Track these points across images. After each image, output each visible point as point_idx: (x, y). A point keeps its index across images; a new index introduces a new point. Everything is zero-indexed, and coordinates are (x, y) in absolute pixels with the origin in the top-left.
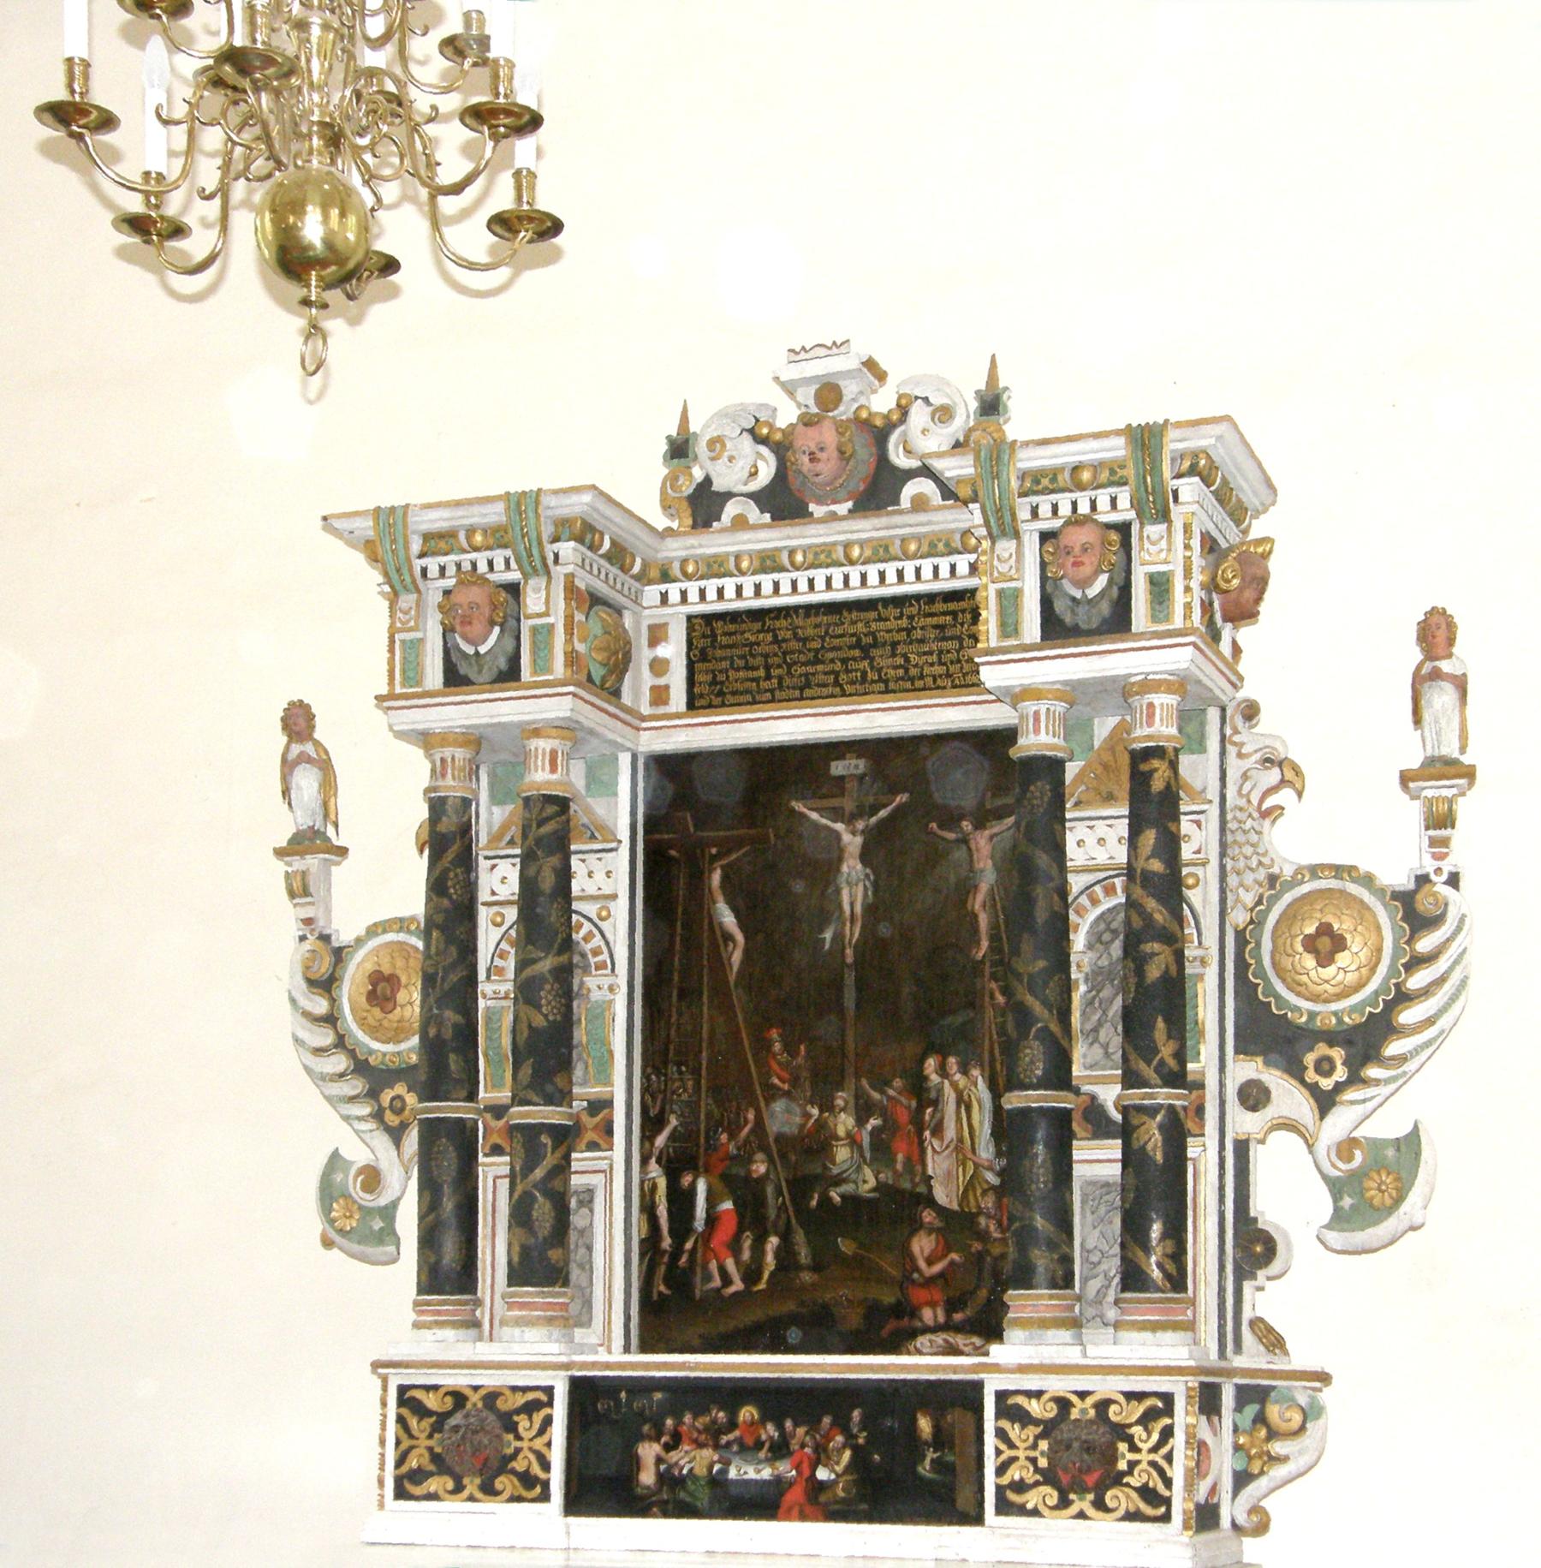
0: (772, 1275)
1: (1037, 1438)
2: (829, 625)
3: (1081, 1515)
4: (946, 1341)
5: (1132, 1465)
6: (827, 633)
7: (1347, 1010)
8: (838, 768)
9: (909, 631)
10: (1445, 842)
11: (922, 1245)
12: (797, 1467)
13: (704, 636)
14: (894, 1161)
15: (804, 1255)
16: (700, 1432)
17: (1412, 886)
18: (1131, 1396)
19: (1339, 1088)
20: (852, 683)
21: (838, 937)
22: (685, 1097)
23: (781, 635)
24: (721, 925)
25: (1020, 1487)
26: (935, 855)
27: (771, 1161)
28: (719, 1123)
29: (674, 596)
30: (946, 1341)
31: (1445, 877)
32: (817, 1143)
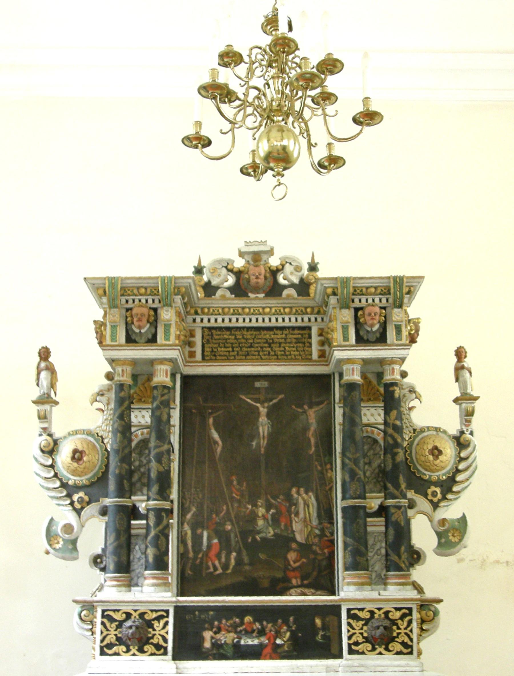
0: (234, 567)
1: (363, 625)
2: (256, 335)
3: (380, 653)
4: (301, 591)
5: (399, 634)
6: (255, 337)
7: (442, 475)
8: (257, 384)
9: (285, 339)
10: (470, 421)
11: (292, 556)
12: (269, 639)
13: (209, 335)
14: (281, 525)
15: (246, 559)
16: (229, 627)
17: (458, 435)
18: (397, 609)
19: (440, 501)
20: (265, 355)
21: (258, 444)
22: (199, 500)
23: (238, 337)
24: (213, 438)
25: (357, 644)
26: (295, 417)
27: (233, 524)
28: (212, 511)
29: (198, 320)
30: (301, 591)
31: (469, 432)
32: (253, 518)
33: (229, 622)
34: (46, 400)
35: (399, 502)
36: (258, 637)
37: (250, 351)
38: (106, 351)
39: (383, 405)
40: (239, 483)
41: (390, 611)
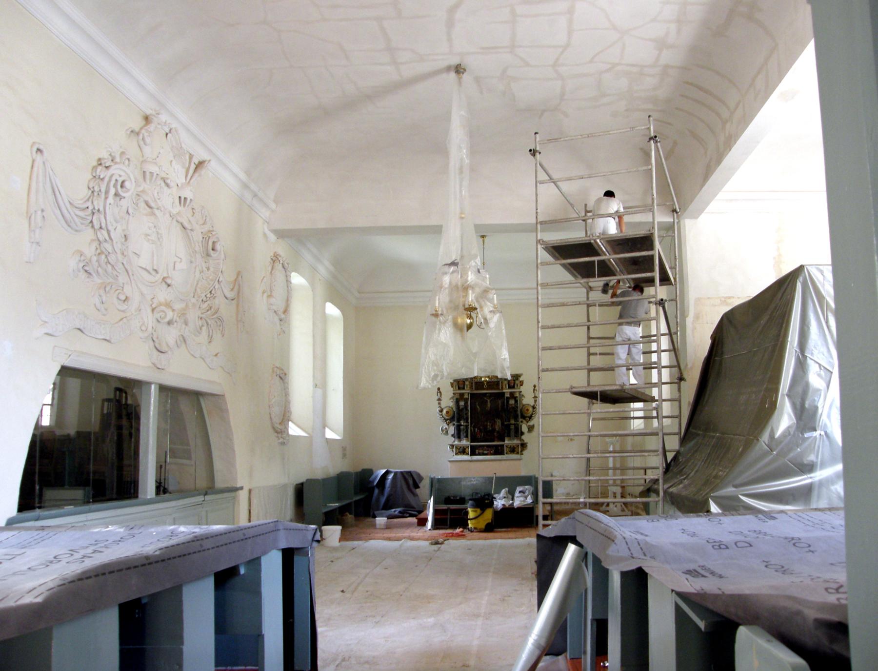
34: (439, 400)
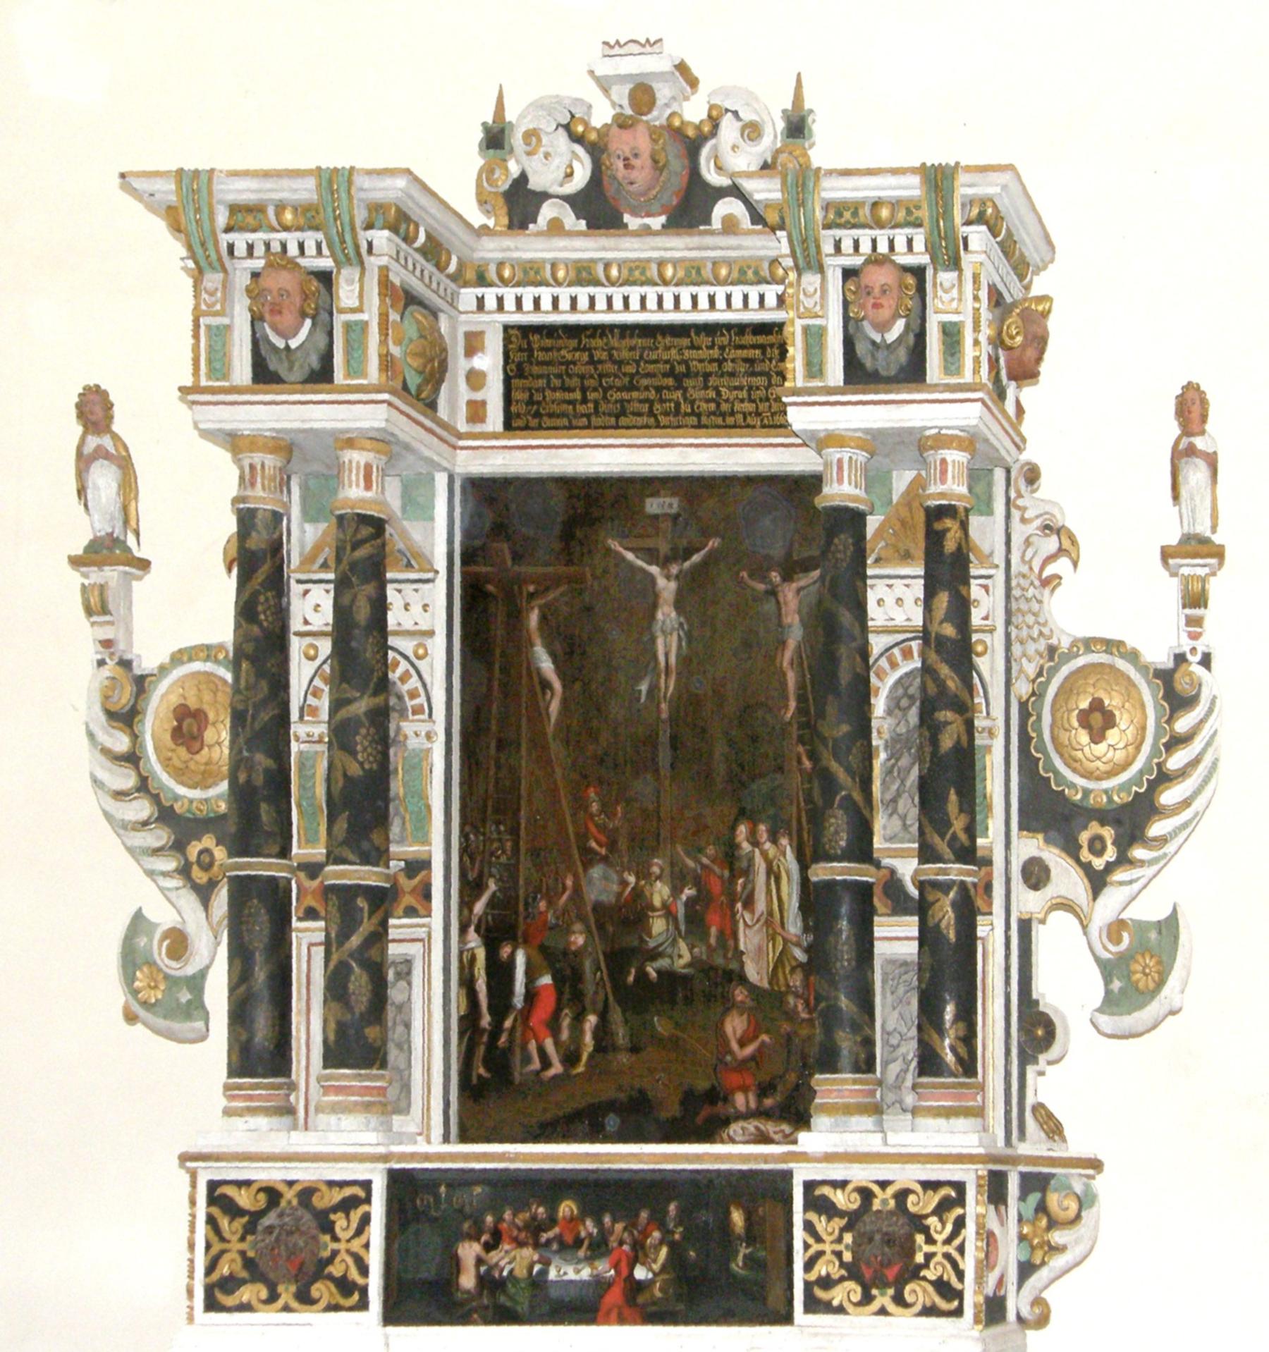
1: (843, 1230)
2: (643, 349)
3: (883, 1311)
4: (757, 1128)
5: (929, 1257)
6: (641, 357)
7: (1112, 789)
8: (653, 506)
9: (720, 362)
11: (735, 1025)
12: (616, 1266)
13: (521, 350)
17: (1171, 665)
19: (1109, 868)
20: (666, 414)
21: (653, 689)
23: (598, 355)
24: (538, 670)
25: (827, 1283)
27: (588, 931)
28: (538, 890)
30: (757, 1128)
31: (1198, 657)
32: (631, 913)
33: (521, 1216)
35: (945, 872)
36: (590, 1260)
37: (629, 401)
38: (197, 408)
39: (922, 573)
40: (604, 809)
41: (912, 1192)
